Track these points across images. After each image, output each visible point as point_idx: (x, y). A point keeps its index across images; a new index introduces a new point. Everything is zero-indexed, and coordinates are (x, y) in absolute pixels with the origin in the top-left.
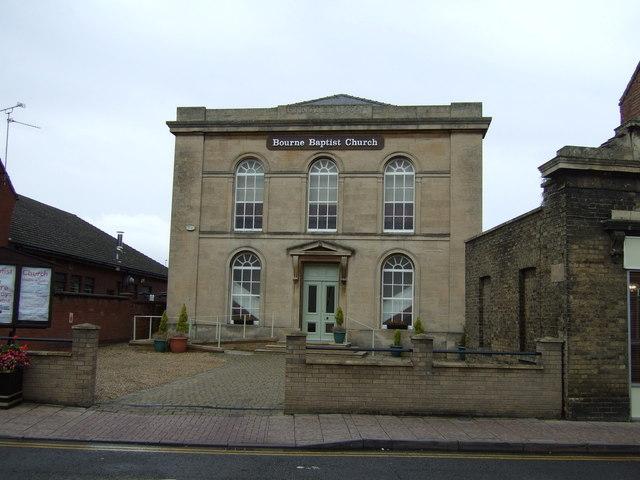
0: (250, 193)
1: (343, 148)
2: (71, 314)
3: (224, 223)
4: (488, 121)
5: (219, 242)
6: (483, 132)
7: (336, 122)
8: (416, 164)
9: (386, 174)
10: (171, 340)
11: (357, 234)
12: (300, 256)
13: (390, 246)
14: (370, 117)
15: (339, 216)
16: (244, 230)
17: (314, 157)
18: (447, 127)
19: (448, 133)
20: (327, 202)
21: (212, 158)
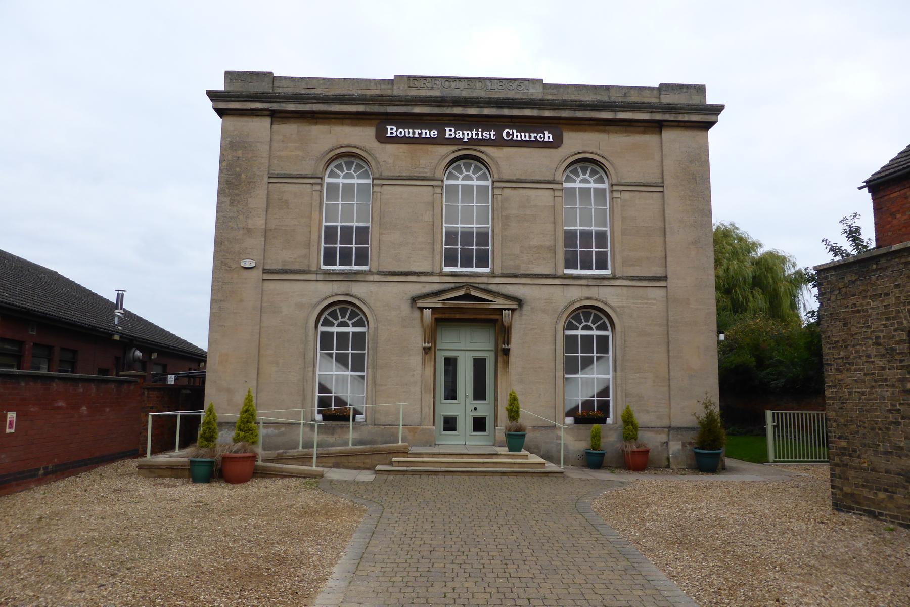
0: (347, 211)
1: (499, 143)
2: (12, 416)
4: (718, 109)
5: (298, 286)
6: (709, 125)
8: (373, 164)
9: (446, 182)
10: (225, 459)
11: (525, 276)
12: (434, 309)
13: (576, 295)
14: (540, 97)
15: (372, 247)
16: (337, 267)
17: (453, 156)
18: (658, 117)
19: (658, 126)
20: (474, 226)
21: (283, 154)
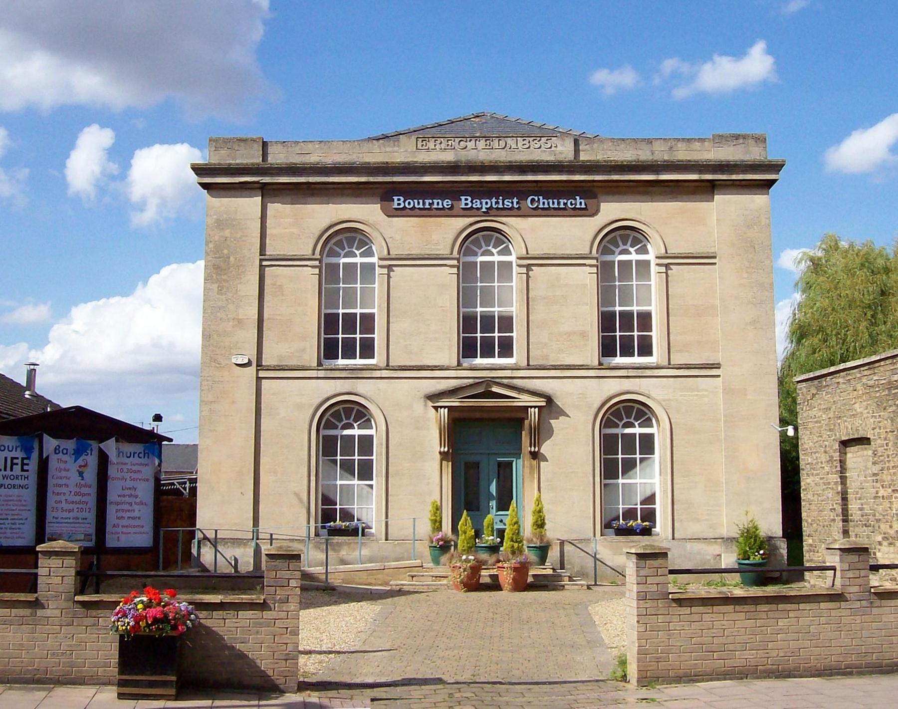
12: (449, 408)
19: (708, 189)
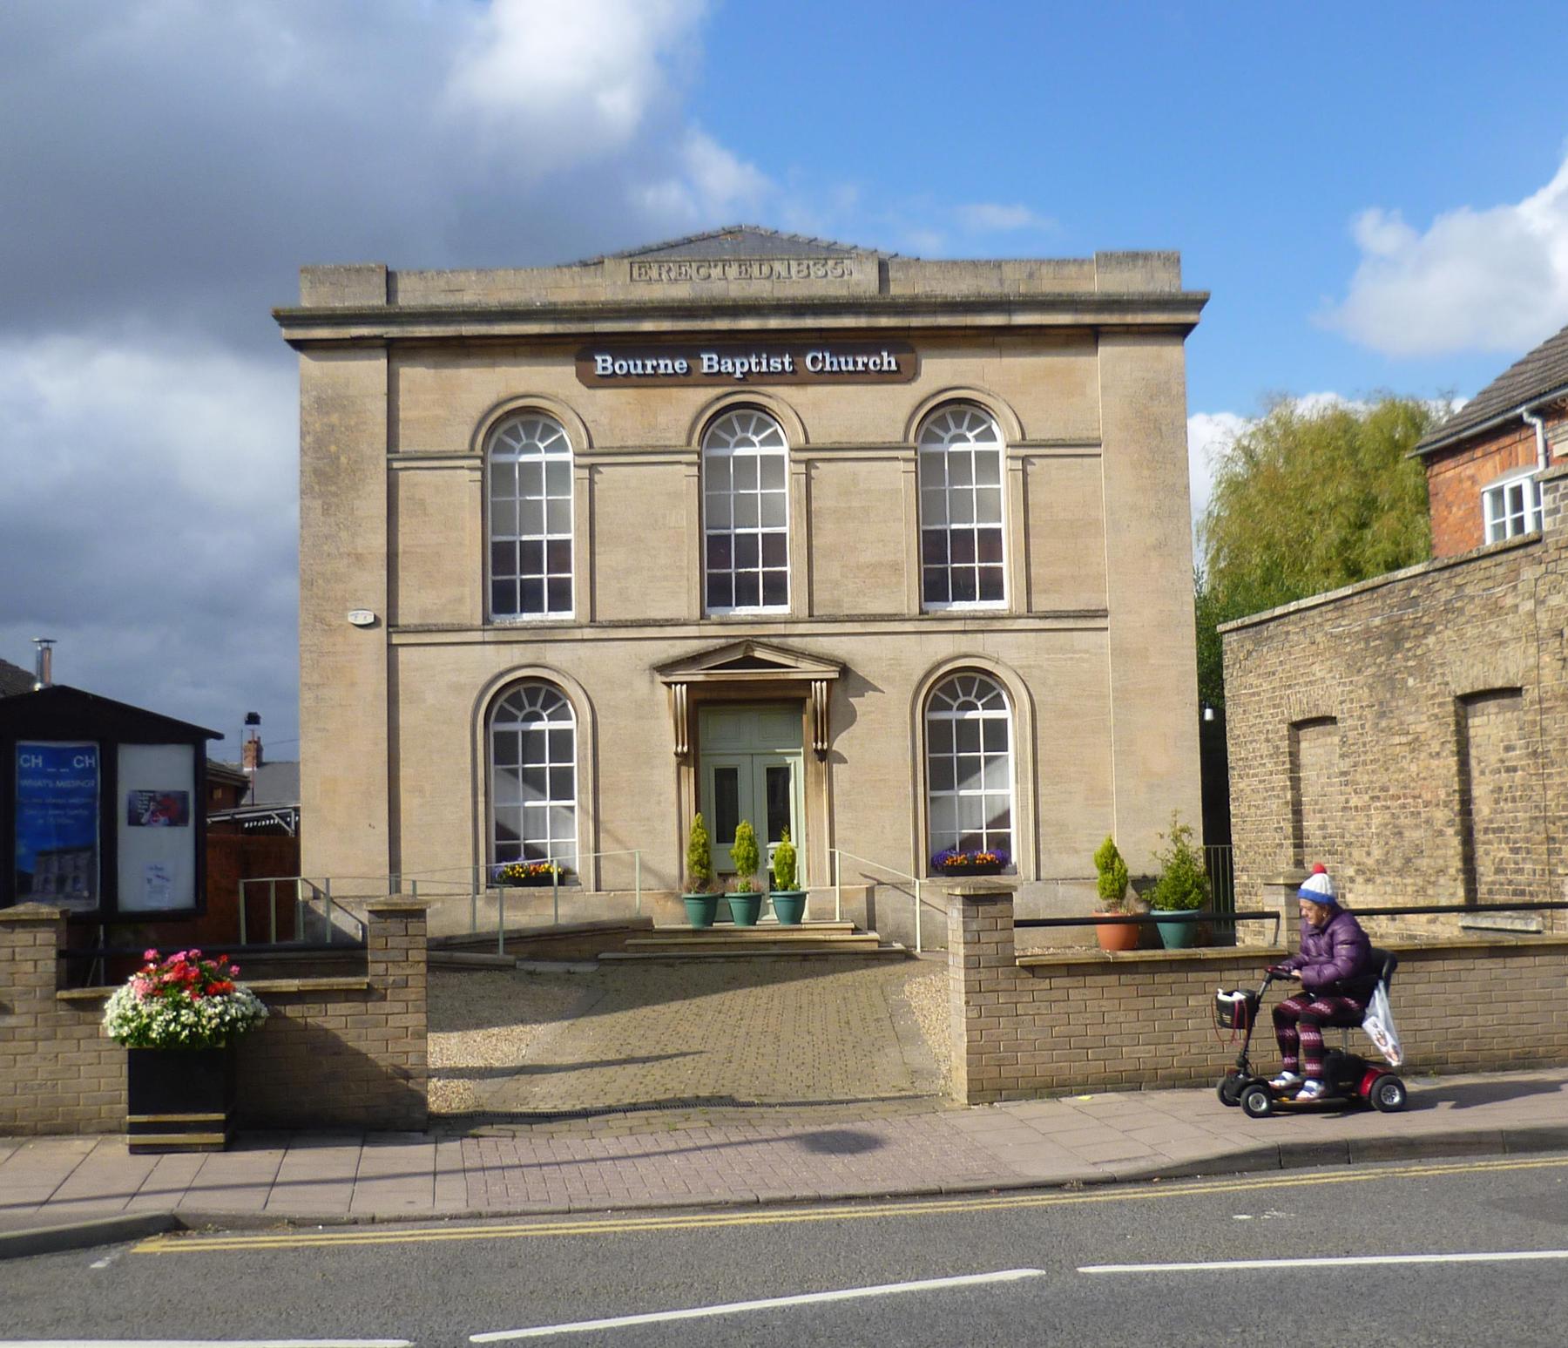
1: (795, 378)
3: (460, 600)
7: (780, 308)
18: (1089, 319)
19: (1089, 337)
